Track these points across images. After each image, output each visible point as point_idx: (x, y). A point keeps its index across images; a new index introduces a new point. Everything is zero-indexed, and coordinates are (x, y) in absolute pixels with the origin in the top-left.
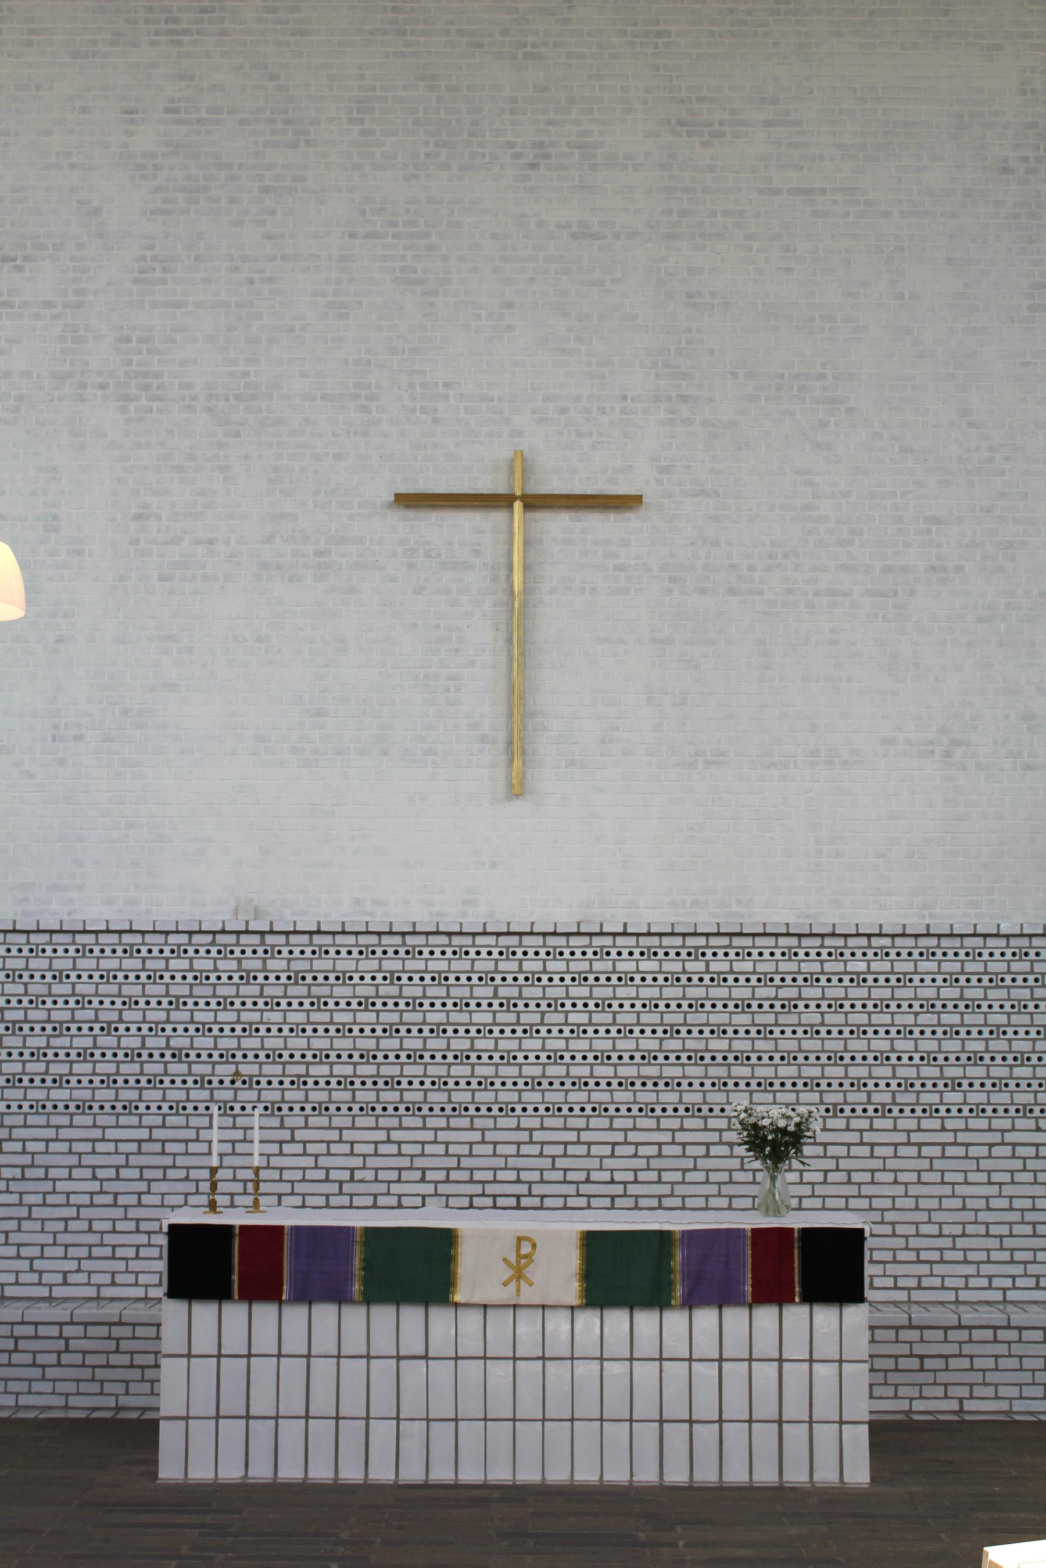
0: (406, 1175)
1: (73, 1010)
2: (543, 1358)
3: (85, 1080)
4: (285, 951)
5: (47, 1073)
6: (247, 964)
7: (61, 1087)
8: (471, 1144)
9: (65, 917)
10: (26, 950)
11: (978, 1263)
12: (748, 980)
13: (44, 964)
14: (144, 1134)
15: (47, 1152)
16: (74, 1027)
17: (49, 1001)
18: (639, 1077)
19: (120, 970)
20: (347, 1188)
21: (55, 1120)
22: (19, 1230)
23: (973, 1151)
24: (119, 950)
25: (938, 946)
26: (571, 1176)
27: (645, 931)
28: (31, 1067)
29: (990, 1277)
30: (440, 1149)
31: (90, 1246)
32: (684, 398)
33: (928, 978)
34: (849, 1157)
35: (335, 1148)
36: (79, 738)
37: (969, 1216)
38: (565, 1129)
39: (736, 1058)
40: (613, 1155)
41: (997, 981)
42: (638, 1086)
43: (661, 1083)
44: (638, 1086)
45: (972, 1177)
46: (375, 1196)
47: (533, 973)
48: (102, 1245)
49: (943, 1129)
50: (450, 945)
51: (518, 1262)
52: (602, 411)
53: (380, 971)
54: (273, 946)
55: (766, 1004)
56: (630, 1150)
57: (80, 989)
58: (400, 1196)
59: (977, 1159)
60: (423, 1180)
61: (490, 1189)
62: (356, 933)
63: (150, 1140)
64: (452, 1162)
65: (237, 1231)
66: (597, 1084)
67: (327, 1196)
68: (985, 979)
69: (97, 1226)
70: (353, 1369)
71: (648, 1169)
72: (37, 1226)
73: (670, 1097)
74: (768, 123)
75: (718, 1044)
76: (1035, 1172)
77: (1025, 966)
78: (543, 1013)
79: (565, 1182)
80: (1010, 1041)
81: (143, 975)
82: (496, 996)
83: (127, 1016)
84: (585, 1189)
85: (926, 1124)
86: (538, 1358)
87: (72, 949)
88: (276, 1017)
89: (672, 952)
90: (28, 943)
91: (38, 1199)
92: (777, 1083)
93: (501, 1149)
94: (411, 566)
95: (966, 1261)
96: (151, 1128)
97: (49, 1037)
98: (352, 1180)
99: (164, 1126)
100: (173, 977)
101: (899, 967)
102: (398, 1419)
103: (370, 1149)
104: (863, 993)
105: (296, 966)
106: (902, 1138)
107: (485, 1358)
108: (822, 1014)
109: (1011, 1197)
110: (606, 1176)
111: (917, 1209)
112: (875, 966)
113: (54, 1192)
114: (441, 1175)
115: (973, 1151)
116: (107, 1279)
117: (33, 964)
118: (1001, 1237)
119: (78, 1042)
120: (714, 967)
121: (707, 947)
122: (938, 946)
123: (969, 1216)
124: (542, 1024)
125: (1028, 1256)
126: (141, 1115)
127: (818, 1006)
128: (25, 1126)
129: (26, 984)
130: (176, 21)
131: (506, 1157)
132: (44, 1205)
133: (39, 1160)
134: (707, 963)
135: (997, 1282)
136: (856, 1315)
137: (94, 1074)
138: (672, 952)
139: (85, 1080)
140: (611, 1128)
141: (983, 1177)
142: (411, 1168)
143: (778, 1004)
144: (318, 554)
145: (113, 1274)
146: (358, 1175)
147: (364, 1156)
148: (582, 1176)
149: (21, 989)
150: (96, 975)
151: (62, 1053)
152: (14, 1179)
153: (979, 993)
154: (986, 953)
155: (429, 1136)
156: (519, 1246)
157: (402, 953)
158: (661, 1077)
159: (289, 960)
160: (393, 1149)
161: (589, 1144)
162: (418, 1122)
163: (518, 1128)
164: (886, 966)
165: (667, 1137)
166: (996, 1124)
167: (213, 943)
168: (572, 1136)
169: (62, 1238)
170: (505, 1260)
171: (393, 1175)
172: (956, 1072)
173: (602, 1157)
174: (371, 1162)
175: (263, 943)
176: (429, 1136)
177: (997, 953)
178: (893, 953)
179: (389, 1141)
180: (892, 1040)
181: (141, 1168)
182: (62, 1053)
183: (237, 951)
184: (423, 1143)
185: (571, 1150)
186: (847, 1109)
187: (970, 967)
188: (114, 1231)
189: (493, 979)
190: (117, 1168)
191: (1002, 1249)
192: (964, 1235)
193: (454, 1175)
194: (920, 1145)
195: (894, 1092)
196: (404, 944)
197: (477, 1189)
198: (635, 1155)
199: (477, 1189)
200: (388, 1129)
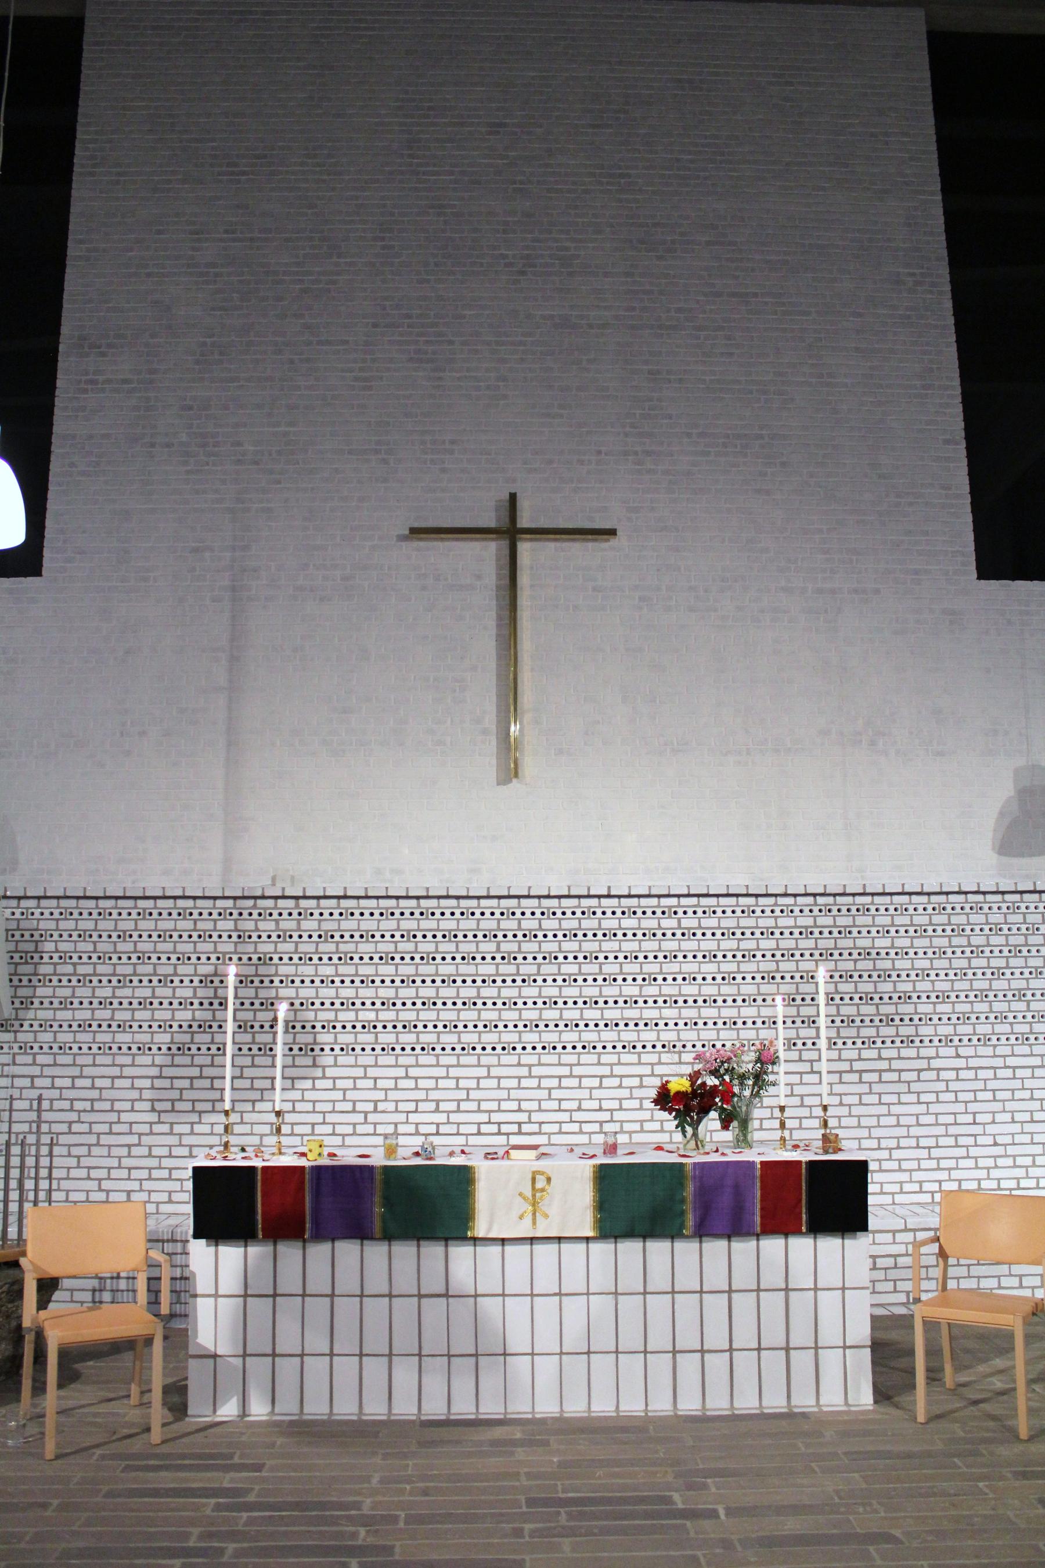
0: (422, 1106)
1: (135, 964)
2: (560, 1294)
3: (145, 1025)
4: (316, 913)
5: (112, 1019)
6: (283, 925)
7: (124, 1031)
8: (478, 1079)
9: (129, 885)
10: (95, 912)
11: (911, 1171)
12: (713, 934)
13: (110, 925)
14: (195, 1072)
15: (112, 1088)
16: (135, 979)
17: (115, 957)
18: (623, 1019)
19: (175, 930)
20: (371, 1118)
21: (120, 1060)
22: (89, 1155)
23: (905, 1076)
24: (175, 913)
25: (872, 903)
26: (565, 1105)
27: (626, 893)
28: (98, 1014)
29: (921, 1183)
30: (452, 1083)
31: (150, 1169)
32: (648, 453)
33: (864, 930)
34: (801, 1083)
35: (360, 1083)
36: (143, 733)
37: (903, 1131)
38: (560, 1064)
39: (705, 1001)
40: (600, 1087)
41: (921, 931)
42: (621, 1026)
43: (641, 1024)
44: (621, 1026)
45: (904, 1098)
46: (396, 1124)
47: (530, 930)
48: (160, 1168)
49: (880, 1058)
50: (458, 907)
51: (534, 1196)
52: (581, 462)
53: (398, 929)
54: (306, 909)
55: (729, 955)
56: (616, 1082)
57: (141, 947)
58: (417, 1124)
59: (909, 1083)
60: (437, 1110)
61: (496, 1117)
62: (377, 898)
63: (201, 1077)
64: (463, 1095)
65: (378, 1177)
66: (586, 1025)
67: (354, 1125)
68: (911, 930)
69: (156, 1151)
70: (375, 1308)
71: (631, 1098)
72: (104, 1151)
73: (649, 1036)
74: (708, 243)
75: (689, 990)
76: (956, 1092)
77: (944, 919)
78: (539, 965)
79: (560, 1110)
80: (933, 982)
81: (195, 935)
82: (498, 951)
83: (181, 969)
84: (577, 1116)
85: (865, 1054)
86: (555, 1294)
87: (134, 912)
88: (309, 970)
89: (649, 912)
90: (97, 907)
91: (105, 1128)
92: (740, 1022)
93: (504, 1083)
94: (424, 588)
95: (900, 1170)
96: (201, 1066)
97: (114, 987)
98: (375, 1111)
99: (212, 1065)
100: (220, 936)
101: (841, 921)
102: (420, 1355)
103: (391, 1084)
104: (811, 943)
105: (326, 926)
106: (845, 1066)
107: (503, 1295)
108: (777, 962)
109: (937, 1114)
110: (595, 1105)
111: (859, 1126)
112: (821, 921)
113: (119, 1122)
114: (453, 1106)
115: (905, 1076)
116: (165, 1197)
117: (102, 925)
118: (929, 1148)
119: (139, 993)
120: (685, 923)
121: (679, 906)
122: (872, 903)
123: (903, 1131)
124: (538, 974)
125: (952, 1163)
126: (193, 1056)
127: (773, 956)
128: (94, 1065)
129: (95, 943)
130: (236, 165)
131: (509, 1089)
132: (111, 1133)
133: (106, 1094)
134: (679, 920)
135: (926, 1187)
136: (858, 1246)
137: (153, 1020)
138: (649, 912)
139: (145, 1025)
140: (599, 1063)
141: (913, 1098)
142: (426, 1100)
143: (739, 955)
144: (345, 579)
145: (170, 1193)
146: (381, 1106)
147: (386, 1090)
148: (574, 1105)
149: (91, 948)
150: (155, 935)
151: (125, 1002)
152: (85, 1111)
153: (907, 942)
154: (911, 908)
155: (442, 1072)
156: (534, 1180)
157: (417, 915)
158: (641, 1019)
159: (320, 921)
160: (411, 1084)
161: (580, 1077)
162: (432, 1060)
163: (519, 1064)
164: (829, 921)
165: (647, 1070)
166: (923, 1052)
167: (255, 907)
168: (565, 1071)
169: (125, 1162)
170: (520, 1194)
171: (411, 1106)
172: (890, 1009)
173: (591, 1088)
174: (393, 1095)
175: (297, 906)
176: (442, 1072)
177: (920, 908)
178: (835, 909)
179: (407, 1077)
180: (836, 983)
181: (194, 1101)
182: (125, 1002)
183: (275, 913)
184: (437, 1079)
185: (565, 1082)
186: (799, 1043)
187: (898, 920)
188: (170, 1156)
189: (495, 936)
190: (173, 1101)
191: (930, 1158)
192: (898, 1147)
193: (464, 1106)
194: (861, 1072)
195: (838, 1028)
196: (419, 907)
197: (484, 1117)
198: (620, 1086)
199: (484, 1117)
200: (407, 1067)
